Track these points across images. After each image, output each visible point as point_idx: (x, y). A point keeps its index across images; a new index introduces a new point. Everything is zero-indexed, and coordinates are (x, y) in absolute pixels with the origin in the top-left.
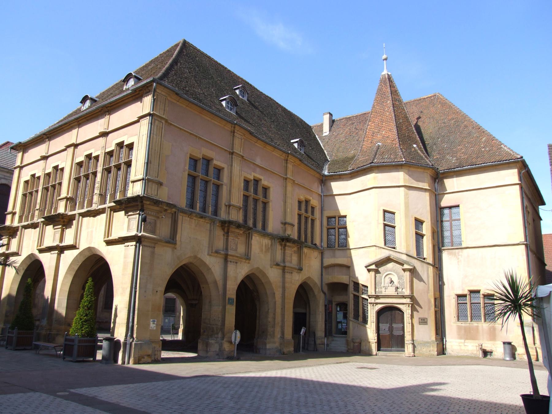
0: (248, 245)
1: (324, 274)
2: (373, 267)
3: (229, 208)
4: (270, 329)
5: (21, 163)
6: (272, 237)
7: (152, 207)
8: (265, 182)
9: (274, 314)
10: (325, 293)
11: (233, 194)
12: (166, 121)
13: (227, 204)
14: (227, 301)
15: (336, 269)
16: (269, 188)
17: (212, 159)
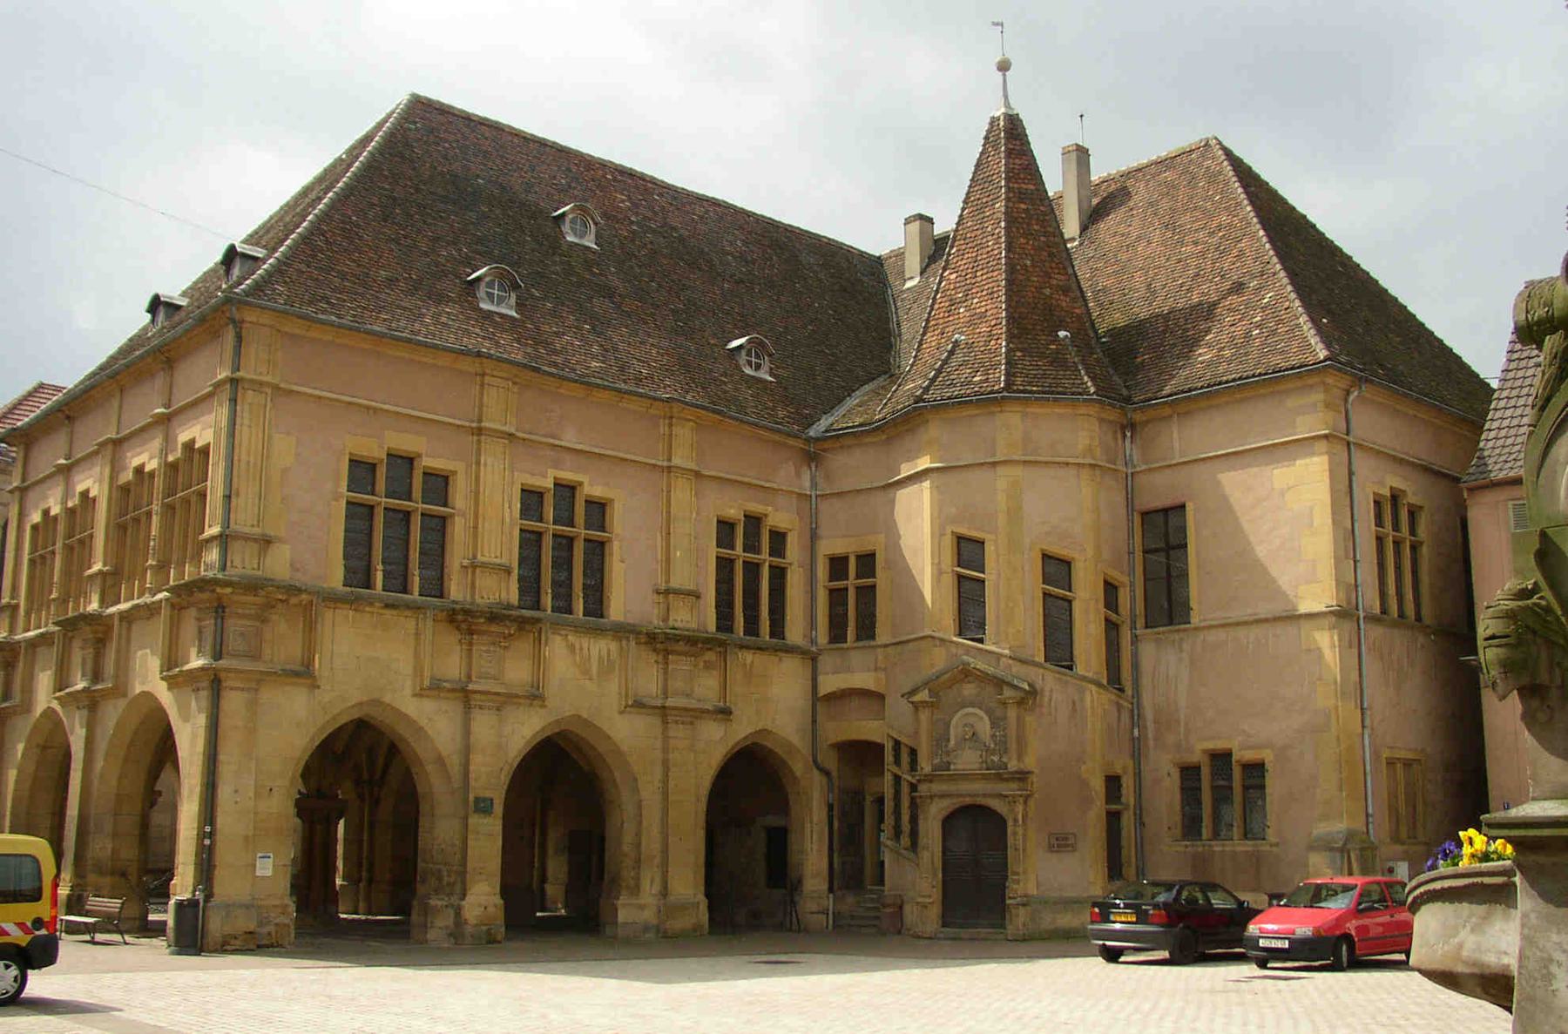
0: (538, 660)
1: (819, 718)
2: (923, 696)
3: (474, 573)
4: (628, 874)
5: (23, 480)
6: (622, 631)
7: (243, 598)
8: (593, 488)
9: (638, 834)
10: (827, 773)
11: (486, 535)
12: (276, 388)
13: (466, 562)
14: (471, 803)
15: (855, 702)
16: (612, 501)
17: (420, 456)
